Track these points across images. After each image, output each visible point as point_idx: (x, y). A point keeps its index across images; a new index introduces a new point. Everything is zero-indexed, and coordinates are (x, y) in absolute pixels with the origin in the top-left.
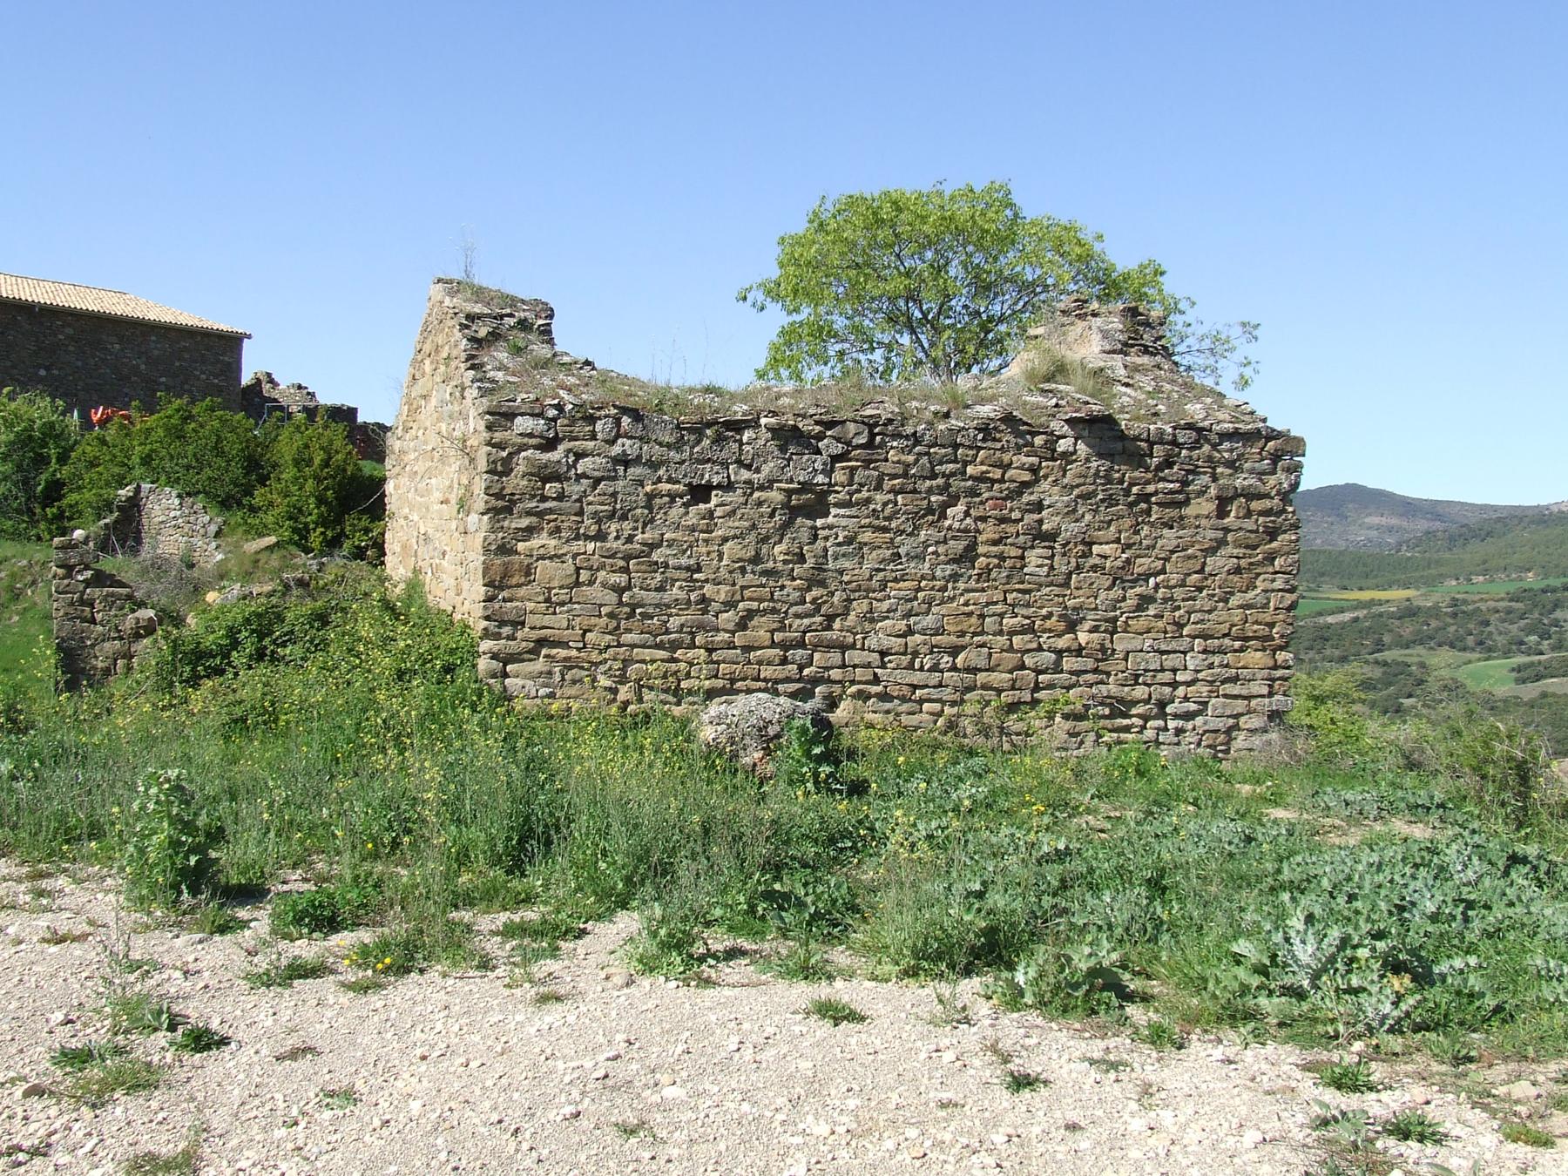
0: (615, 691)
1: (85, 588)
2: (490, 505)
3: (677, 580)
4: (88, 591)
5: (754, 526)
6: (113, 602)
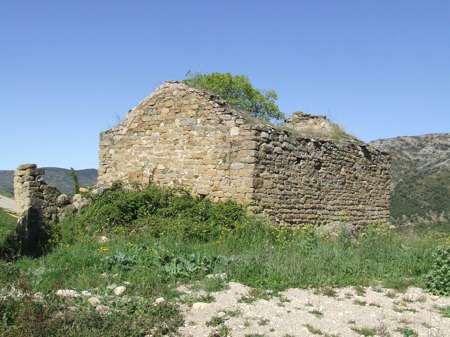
0: (279, 223)
1: (40, 185)
2: (256, 161)
3: (293, 187)
4: (41, 186)
5: (309, 172)
6: (50, 191)
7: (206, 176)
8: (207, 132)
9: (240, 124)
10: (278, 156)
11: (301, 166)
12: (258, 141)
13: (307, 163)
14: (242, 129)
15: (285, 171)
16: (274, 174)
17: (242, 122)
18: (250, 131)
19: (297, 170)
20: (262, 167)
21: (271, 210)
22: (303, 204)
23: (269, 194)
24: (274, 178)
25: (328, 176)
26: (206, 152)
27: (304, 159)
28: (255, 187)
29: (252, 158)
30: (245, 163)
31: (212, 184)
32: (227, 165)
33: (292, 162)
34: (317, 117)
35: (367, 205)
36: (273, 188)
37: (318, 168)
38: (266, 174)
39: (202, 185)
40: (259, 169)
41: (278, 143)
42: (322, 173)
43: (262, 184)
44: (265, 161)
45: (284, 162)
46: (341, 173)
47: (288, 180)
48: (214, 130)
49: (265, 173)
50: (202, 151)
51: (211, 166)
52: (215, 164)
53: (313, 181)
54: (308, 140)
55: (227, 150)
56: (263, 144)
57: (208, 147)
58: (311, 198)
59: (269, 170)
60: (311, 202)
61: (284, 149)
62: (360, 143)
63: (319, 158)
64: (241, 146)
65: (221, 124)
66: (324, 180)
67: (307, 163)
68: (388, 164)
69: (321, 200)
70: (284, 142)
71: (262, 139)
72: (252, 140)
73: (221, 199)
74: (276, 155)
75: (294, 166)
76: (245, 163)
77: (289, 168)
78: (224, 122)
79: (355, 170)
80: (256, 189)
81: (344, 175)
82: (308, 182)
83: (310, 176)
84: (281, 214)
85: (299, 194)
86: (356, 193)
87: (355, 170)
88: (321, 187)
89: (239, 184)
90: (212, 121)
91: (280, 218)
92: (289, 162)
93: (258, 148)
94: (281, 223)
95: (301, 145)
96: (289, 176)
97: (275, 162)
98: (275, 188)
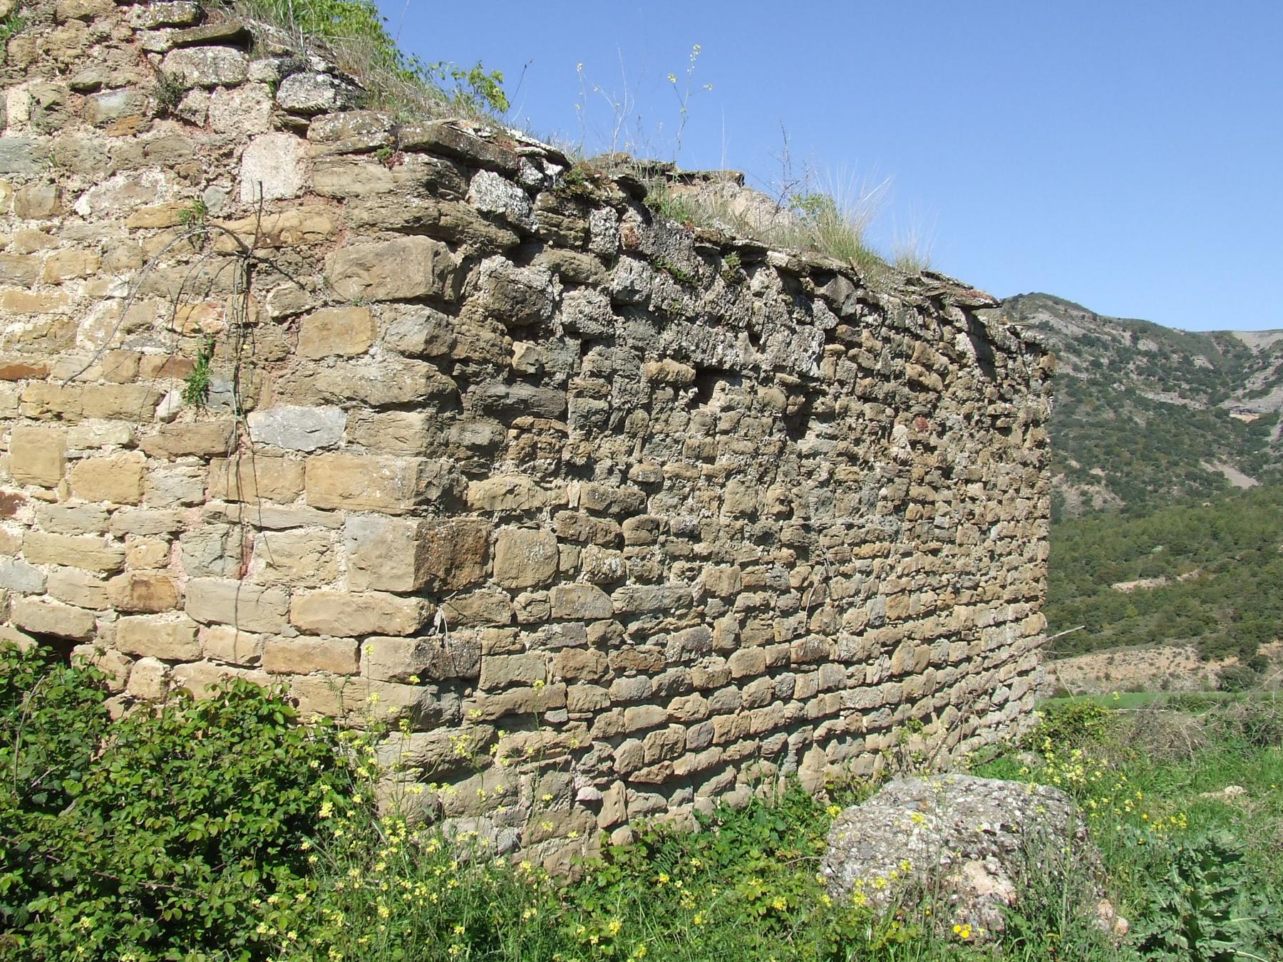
0: (595, 806)
2: (434, 387)
3: (675, 558)
5: (756, 453)
7: (74, 501)
8: (75, 183)
9: (309, 114)
10: (584, 350)
11: (716, 420)
12: (449, 236)
13: (749, 398)
14: (323, 148)
15: (630, 452)
16: (559, 482)
17: (330, 93)
18: (387, 162)
19: (695, 442)
20: (484, 432)
21: (549, 735)
22: (726, 653)
23: (531, 627)
24: (565, 507)
25: (843, 471)
26: (70, 323)
27: (733, 375)
28: (431, 592)
29: (408, 368)
30: (351, 402)
31: (111, 561)
32: (218, 419)
33: (670, 391)
34: (706, 178)
35: (981, 601)
36: (558, 576)
37: (796, 425)
38: (510, 480)
39: (45, 570)
40: (462, 453)
41: (586, 261)
42: (814, 455)
43: (486, 558)
44: (501, 389)
45: (622, 391)
46: (894, 450)
47: (645, 511)
48: (126, 164)
49: (505, 475)
50: (42, 320)
51: (107, 425)
52: (129, 416)
53: (778, 508)
54: (753, 257)
55: (213, 314)
56: (487, 265)
57: (81, 290)
58: (766, 607)
59: (532, 456)
60: (767, 634)
61: (623, 304)
62: (960, 291)
63: (804, 367)
64: (318, 279)
65: (170, 124)
66: (825, 492)
67: (749, 398)
68: (1043, 398)
69: (811, 610)
70: (625, 260)
71: (483, 228)
72: (407, 230)
73: (183, 674)
74: (573, 344)
75: (679, 417)
76: (351, 402)
77: (652, 436)
78: (194, 99)
79: (943, 430)
80: (437, 598)
81: (904, 463)
82: (753, 517)
83: (760, 480)
84: (607, 749)
85: (707, 594)
86: (947, 549)
87: (943, 430)
88: (813, 535)
89: (307, 564)
90: (109, 103)
91: (601, 774)
92: (653, 392)
93: (449, 293)
94: (607, 804)
95: (720, 284)
96: (651, 488)
97: (570, 396)
98: (573, 578)
